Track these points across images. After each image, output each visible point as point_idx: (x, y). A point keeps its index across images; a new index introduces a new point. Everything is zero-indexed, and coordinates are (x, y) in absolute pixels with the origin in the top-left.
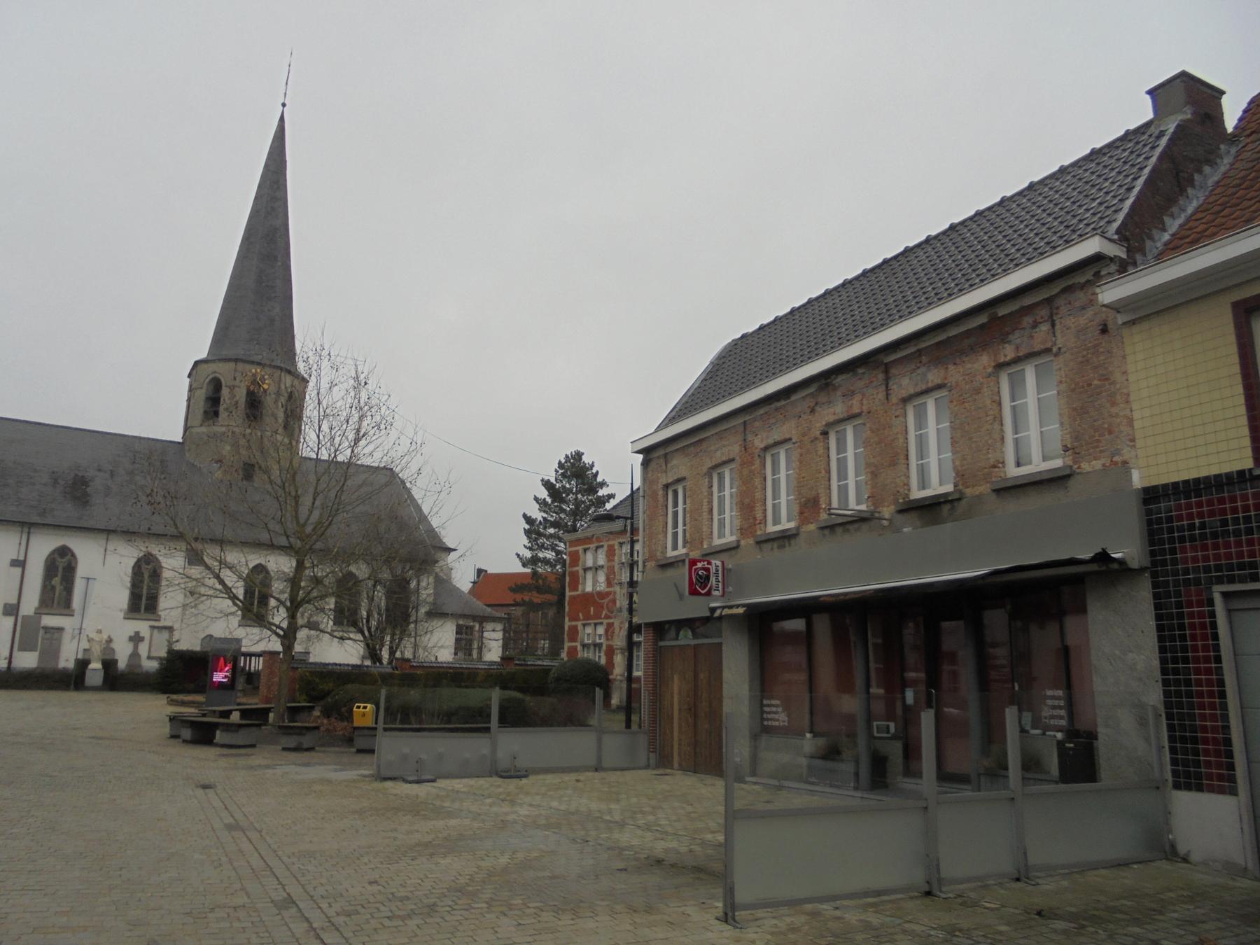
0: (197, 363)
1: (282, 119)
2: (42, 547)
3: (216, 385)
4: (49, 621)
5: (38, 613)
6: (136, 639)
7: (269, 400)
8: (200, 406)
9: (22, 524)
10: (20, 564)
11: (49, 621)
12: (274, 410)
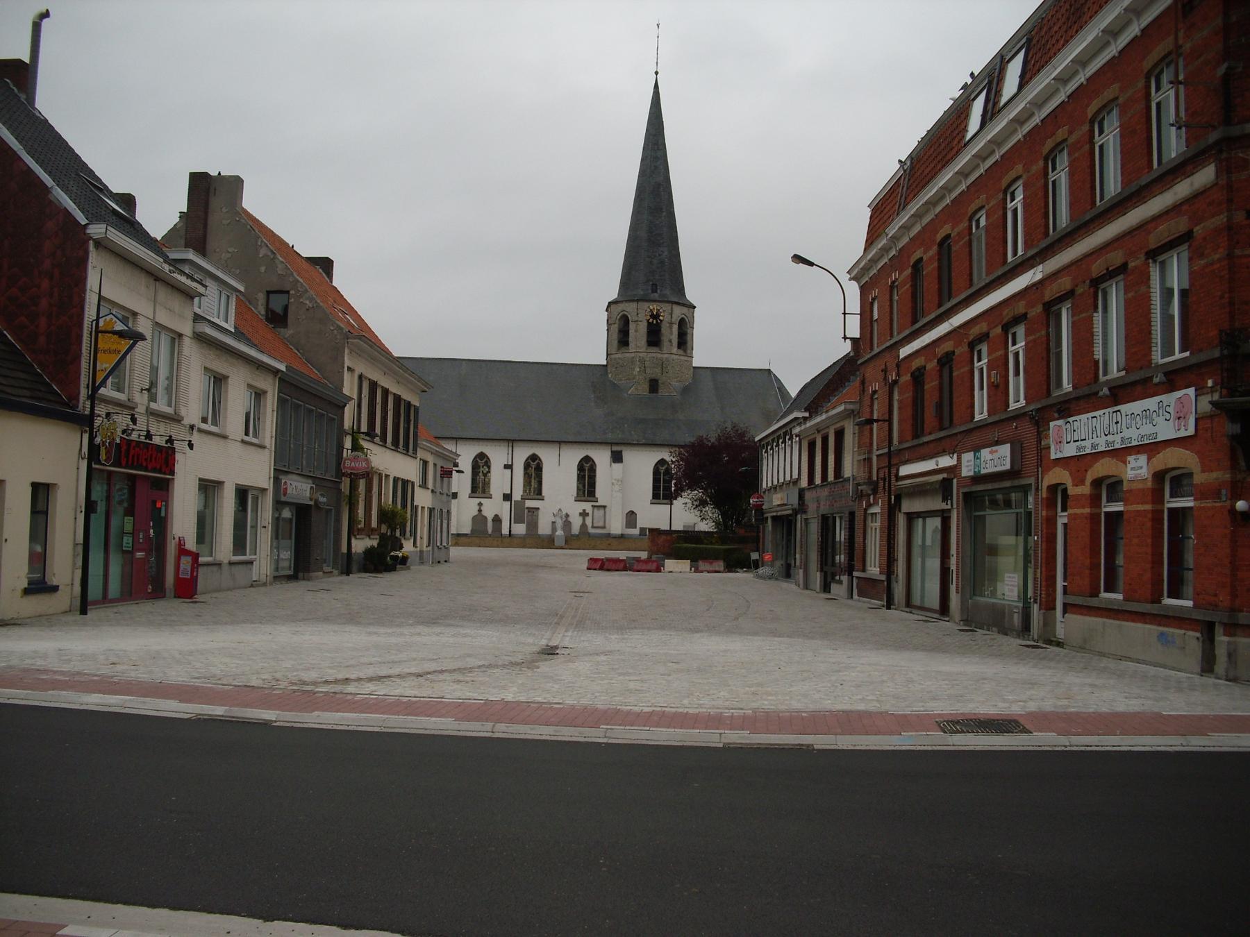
0: (610, 304)
1: (811, 264)
2: (521, 454)
3: (625, 321)
4: (529, 503)
5: (523, 499)
6: (584, 514)
7: (664, 329)
8: (615, 336)
9: (508, 441)
10: (509, 467)
11: (529, 503)
12: (670, 334)
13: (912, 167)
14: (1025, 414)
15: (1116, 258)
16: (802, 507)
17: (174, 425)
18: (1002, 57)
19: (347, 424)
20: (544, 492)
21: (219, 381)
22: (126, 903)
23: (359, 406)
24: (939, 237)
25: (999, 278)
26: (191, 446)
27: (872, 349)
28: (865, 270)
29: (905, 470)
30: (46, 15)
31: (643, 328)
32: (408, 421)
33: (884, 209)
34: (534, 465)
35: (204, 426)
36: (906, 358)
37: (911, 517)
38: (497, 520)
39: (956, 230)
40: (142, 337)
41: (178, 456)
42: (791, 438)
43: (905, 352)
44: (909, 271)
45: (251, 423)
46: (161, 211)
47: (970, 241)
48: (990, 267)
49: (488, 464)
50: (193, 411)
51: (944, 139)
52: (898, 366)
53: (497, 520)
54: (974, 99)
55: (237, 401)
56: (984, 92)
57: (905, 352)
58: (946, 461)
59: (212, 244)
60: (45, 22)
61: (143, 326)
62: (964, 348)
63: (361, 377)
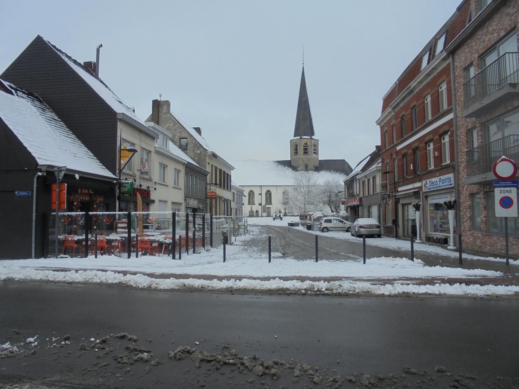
4: (268, 206)
5: (266, 204)
11: (268, 206)
12: (311, 149)
13: (399, 83)
14: (450, 166)
15: (431, 136)
16: (361, 205)
17: (150, 182)
18: (435, 39)
19: (208, 182)
20: (272, 202)
21: (164, 167)
22: (441, 29)
23: (212, 175)
24: (401, 116)
25: (437, 118)
26: (155, 189)
27: (385, 148)
28: (382, 120)
29: (400, 189)
30: (101, 46)
31: (302, 148)
32: (228, 180)
33: (387, 101)
34: (269, 193)
35: (160, 183)
36: (399, 150)
37: (403, 205)
38: (257, 212)
39: (418, 103)
40: (137, 151)
41: (151, 193)
42: (356, 181)
43: (398, 148)
44: (400, 119)
45: (176, 182)
46: (142, 114)
47: (438, 95)
48: (433, 114)
49: (253, 194)
50: (156, 176)
51: (414, 69)
52: (396, 153)
53: (257, 212)
54: (439, 39)
55: (170, 173)
56: (428, 53)
57: (398, 148)
58: (418, 185)
59: (160, 123)
60: (101, 48)
61: (137, 148)
62: (423, 144)
63: (212, 165)
